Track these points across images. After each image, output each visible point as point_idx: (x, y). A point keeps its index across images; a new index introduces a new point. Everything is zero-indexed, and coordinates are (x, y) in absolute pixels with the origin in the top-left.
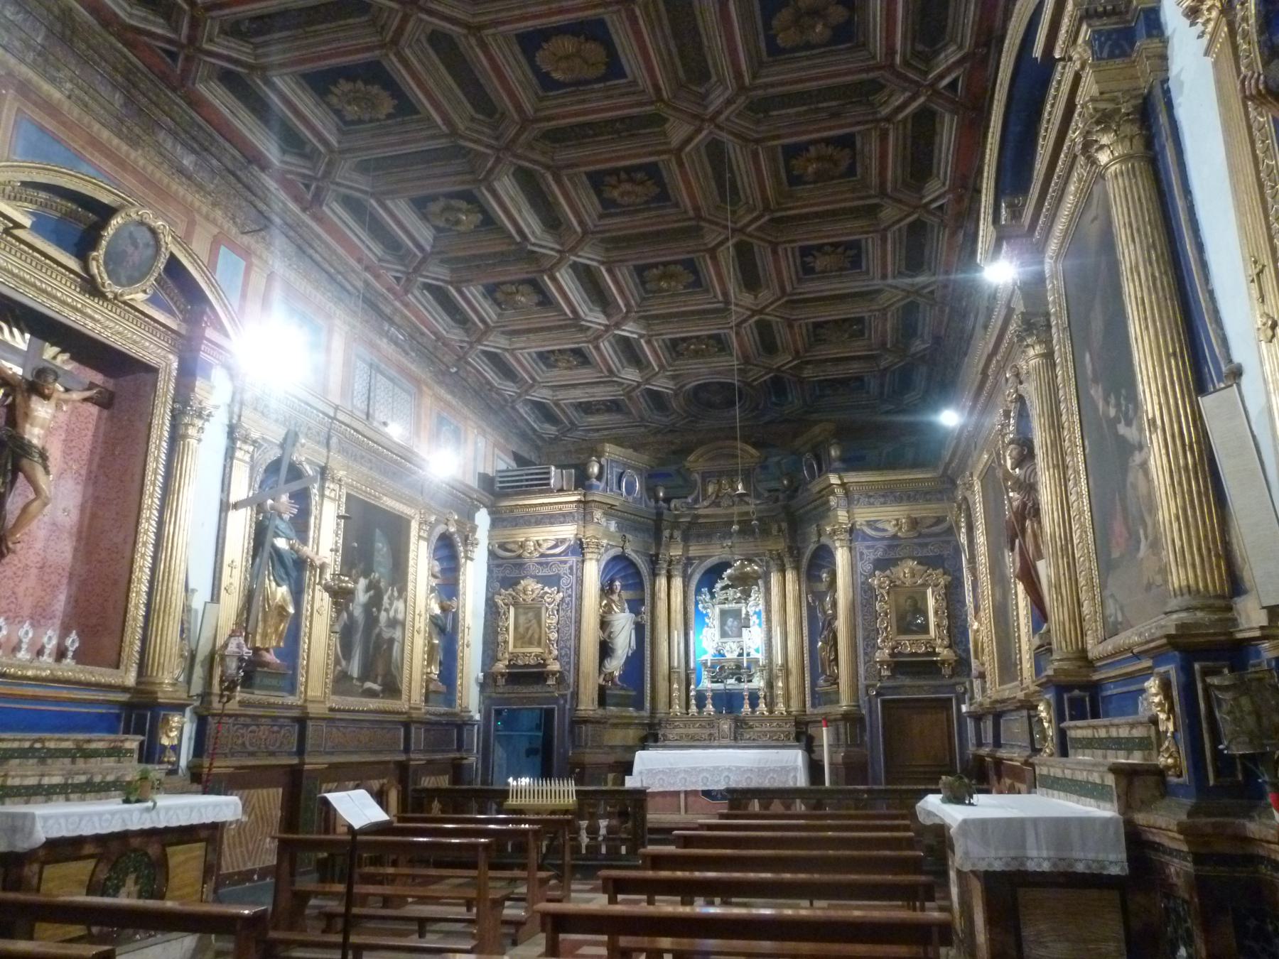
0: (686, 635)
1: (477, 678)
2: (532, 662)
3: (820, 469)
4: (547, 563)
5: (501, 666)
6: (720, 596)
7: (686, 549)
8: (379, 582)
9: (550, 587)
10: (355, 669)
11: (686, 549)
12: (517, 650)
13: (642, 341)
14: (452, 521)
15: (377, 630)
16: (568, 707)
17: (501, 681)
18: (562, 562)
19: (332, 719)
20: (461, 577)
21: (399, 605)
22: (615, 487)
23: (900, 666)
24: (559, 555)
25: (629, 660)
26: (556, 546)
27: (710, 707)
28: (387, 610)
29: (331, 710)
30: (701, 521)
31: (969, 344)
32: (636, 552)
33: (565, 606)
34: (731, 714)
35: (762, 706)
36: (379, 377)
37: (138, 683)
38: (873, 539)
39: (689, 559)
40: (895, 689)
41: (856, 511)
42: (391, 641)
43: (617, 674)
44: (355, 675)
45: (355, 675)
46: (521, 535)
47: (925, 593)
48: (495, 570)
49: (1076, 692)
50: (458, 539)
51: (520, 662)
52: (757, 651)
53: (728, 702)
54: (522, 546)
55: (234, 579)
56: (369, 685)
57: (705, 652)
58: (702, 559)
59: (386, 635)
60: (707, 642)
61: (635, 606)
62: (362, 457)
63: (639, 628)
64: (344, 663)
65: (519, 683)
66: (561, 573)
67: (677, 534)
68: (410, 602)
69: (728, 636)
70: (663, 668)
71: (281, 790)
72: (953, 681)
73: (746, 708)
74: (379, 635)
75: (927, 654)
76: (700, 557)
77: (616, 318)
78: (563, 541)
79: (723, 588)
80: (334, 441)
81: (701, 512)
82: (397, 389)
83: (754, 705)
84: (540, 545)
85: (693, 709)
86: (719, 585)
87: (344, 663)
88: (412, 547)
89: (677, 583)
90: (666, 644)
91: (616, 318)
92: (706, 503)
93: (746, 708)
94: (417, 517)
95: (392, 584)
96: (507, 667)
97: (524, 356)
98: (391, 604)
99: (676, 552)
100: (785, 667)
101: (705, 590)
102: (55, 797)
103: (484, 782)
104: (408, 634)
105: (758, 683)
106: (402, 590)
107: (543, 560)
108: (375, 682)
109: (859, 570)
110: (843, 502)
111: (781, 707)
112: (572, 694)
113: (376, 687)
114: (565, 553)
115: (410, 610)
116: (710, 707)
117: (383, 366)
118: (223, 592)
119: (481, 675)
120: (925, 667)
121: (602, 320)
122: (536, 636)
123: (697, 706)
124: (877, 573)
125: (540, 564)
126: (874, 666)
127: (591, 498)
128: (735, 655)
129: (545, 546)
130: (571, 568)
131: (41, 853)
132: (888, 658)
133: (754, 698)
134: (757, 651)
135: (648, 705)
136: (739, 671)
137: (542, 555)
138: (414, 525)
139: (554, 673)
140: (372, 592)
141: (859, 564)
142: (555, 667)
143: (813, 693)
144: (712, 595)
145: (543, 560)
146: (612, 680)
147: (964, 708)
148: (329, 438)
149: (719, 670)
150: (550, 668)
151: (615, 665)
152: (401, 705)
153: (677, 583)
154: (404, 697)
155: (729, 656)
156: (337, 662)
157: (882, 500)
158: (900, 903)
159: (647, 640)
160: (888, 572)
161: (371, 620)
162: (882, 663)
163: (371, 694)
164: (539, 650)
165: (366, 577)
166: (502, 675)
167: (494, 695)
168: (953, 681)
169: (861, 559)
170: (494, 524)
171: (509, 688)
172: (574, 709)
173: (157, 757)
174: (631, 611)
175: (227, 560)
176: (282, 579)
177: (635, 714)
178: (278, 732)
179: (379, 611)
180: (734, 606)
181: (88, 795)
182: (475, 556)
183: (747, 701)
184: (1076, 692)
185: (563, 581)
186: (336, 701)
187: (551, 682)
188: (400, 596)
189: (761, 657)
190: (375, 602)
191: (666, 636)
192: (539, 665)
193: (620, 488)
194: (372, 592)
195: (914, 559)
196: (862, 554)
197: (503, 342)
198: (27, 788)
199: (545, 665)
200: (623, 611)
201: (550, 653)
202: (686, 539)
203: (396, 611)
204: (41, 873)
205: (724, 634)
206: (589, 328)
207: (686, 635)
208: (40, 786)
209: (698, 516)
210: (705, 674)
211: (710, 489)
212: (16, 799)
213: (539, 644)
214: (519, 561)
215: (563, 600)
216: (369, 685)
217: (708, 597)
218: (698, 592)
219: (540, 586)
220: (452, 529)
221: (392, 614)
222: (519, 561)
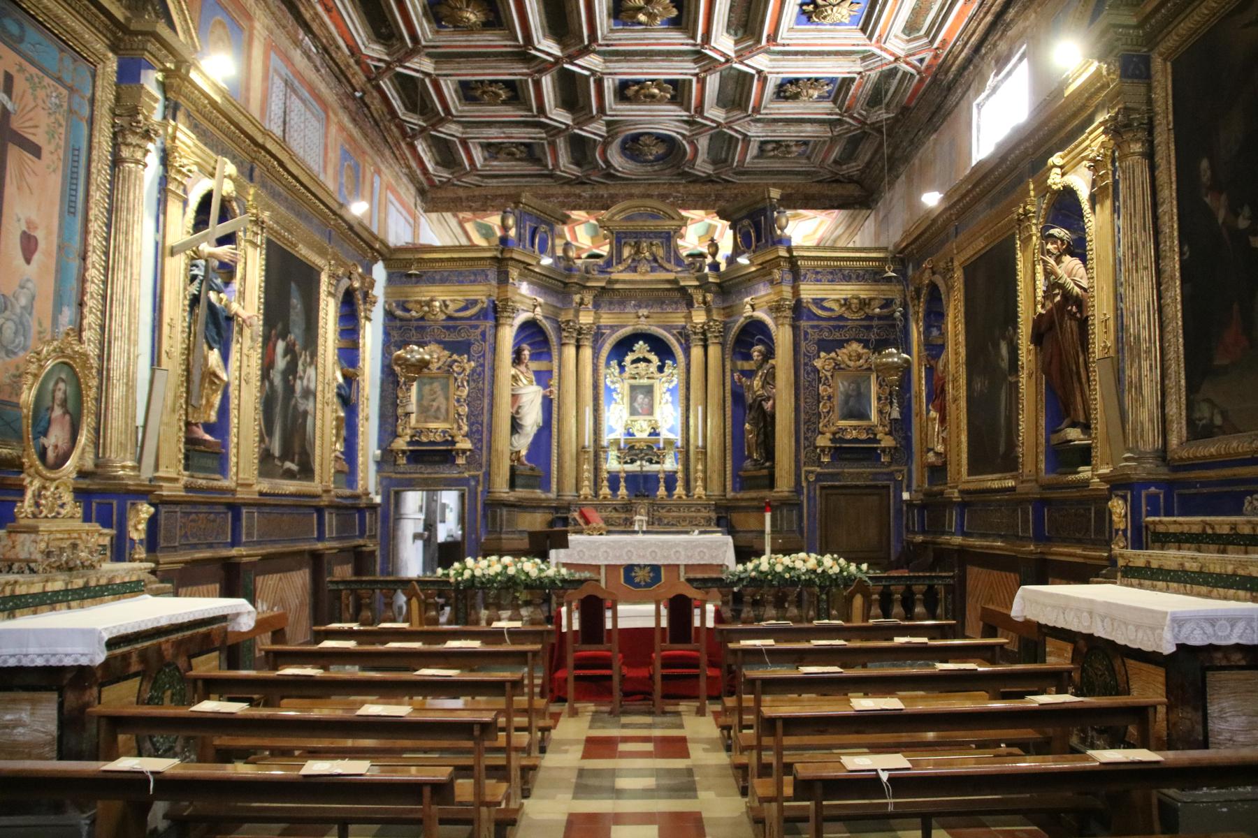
0: (596, 409)
1: (374, 456)
2: (439, 439)
3: (758, 239)
4: (455, 328)
5: (401, 444)
6: (630, 369)
7: (597, 317)
8: (294, 345)
9: (460, 354)
10: (276, 450)
11: (597, 317)
12: (421, 425)
13: (592, 79)
14: (355, 276)
15: (293, 402)
16: (480, 489)
17: (402, 461)
18: (472, 327)
19: (265, 503)
20: (361, 341)
21: (311, 371)
22: (528, 244)
23: (843, 451)
24: (469, 318)
25: (538, 436)
26: (465, 308)
27: (623, 491)
28: (301, 378)
29: (261, 494)
30: (617, 286)
31: (944, 119)
32: (546, 318)
33: (476, 376)
34: (642, 492)
35: (679, 490)
36: (294, 97)
37: (96, 466)
38: (819, 318)
39: (599, 328)
40: (833, 476)
41: (802, 287)
42: (305, 413)
43: (524, 452)
44: (277, 454)
45: (277, 454)
46: (424, 292)
47: (869, 378)
48: (394, 333)
49: (1153, 489)
50: (359, 296)
51: (424, 439)
52: (671, 430)
53: (642, 485)
54: (429, 303)
55: (174, 341)
56: (288, 465)
57: (612, 430)
58: (613, 328)
59: (301, 408)
60: (617, 420)
61: (542, 378)
62: (280, 195)
63: (547, 404)
64: (267, 439)
65: (423, 462)
66: (472, 339)
67: (588, 298)
68: (320, 370)
69: (639, 414)
70: (571, 448)
71: (218, 586)
72: (893, 468)
73: (662, 491)
74: (295, 407)
75: (869, 440)
76: (611, 327)
77: (572, 50)
78: (475, 302)
79: (634, 362)
80: (257, 172)
81: (615, 276)
82: (309, 115)
83: (670, 487)
84: (446, 306)
85: (605, 491)
86: (629, 358)
87: (267, 439)
88: (322, 304)
89: (587, 353)
90: (573, 421)
91: (572, 50)
92: (620, 268)
93: (662, 491)
94: (327, 268)
95: (305, 348)
96: (409, 443)
97: (449, 88)
98: (305, 371)
99: (586, 319)
100: (704, 451)
101: (614, 363)
102: (58, 605)
103: (385, 571)
104: (319, 406)
105: (670, 464)
106: (314, 355)
107: (451, 323)
108: (293, 461)
109: (803, 349)
110: (788, 277)
111: (699, 490)
112: (484, 474)
113: (294, 467)
114: (476, 317)
115: (320, 378)
116: (623, 491)
117: (296, 83)
118: (164, 356)
119: (378, 452)
120: (864, 452)
121: (556, 50)
122: (443, 410)
123: (611, 488)
124: (823, 354)
125: (448, 328)
126: (814, 451)
127: (508, 255)
128: (645, 435)
129: (452, 307)
130: (483, 334)
131: (99, 674)
132: (829, 444)
133: (670, 480)
134: (671, 430)
135: (554, 486)
136: (651, 450)
137: (450, 318)
138: (324, 278)
139: (464, 451)
140: (288, 357)
141: (803, 344)
142: (465, 444)
143: (735, 475)
144: (622, 368)
145: (451, 323)
146: (519, 459)
147: (906, 496)
148: (252, 170)
149: (631, 451)
150: (458, 446)
151: (523, 443)
152: (315, 486)
153: (587, 353)
154: (317, 478)
155: (639, 435)
156: (262, 440)
157: (830, 277)
158: (922, 693)
159: (555, 416)
160: (833, 355)
161: (289, 389)
162: (823, 449)
163: (289, 475)
164: (442, 426)
165: (284, 338)
166: (404, 452)
167: (394, 476)
168: (893, 468)
169: (806, 339)
170: (390, 279)
171: (413, 467)
172: (488, 491)
173: (127, 555)
174: (539, 383)
175: (166, 320)
176: (215, 341)
177: (543, 496)
178: (214, 521)
179: (295, 379)
180: (645, 381)
181: (85, 601)
182: (372, 316)
183: (662, 483)
184: (1153, 489)
185: (474, 348)
186: (265, 485)
187: (461, 461)
188: (311, 363)
189: (678, 438)
190: (291, 369)
191: (574, 413)
192: (446, 442)
193: (533, 244)
194: (288, 357)
195: (859, 341)
196: (806, 333)
197: (427, 65)
198: (34, 595)
199: (453, 443)
200: (531, 382)
201: (460, 428)
202: (597, 306)
203: (309, 379)
204: (100, 693)
205: (633, 412)
206: (536, 57)
207: (596, 409)
208: (45, 593)
209: (610, 282)
210: (613, 453)
211: (626, 252)
212: (25, 610)
213: (446, 420)
214: (422, 323)
215: (473, 371)
216: (288, 465)
217: (618, 370)
218: (608, 365)
219: (447, 353)
220: (357, 285)
221: (305, 382)
222: (422, 323)
